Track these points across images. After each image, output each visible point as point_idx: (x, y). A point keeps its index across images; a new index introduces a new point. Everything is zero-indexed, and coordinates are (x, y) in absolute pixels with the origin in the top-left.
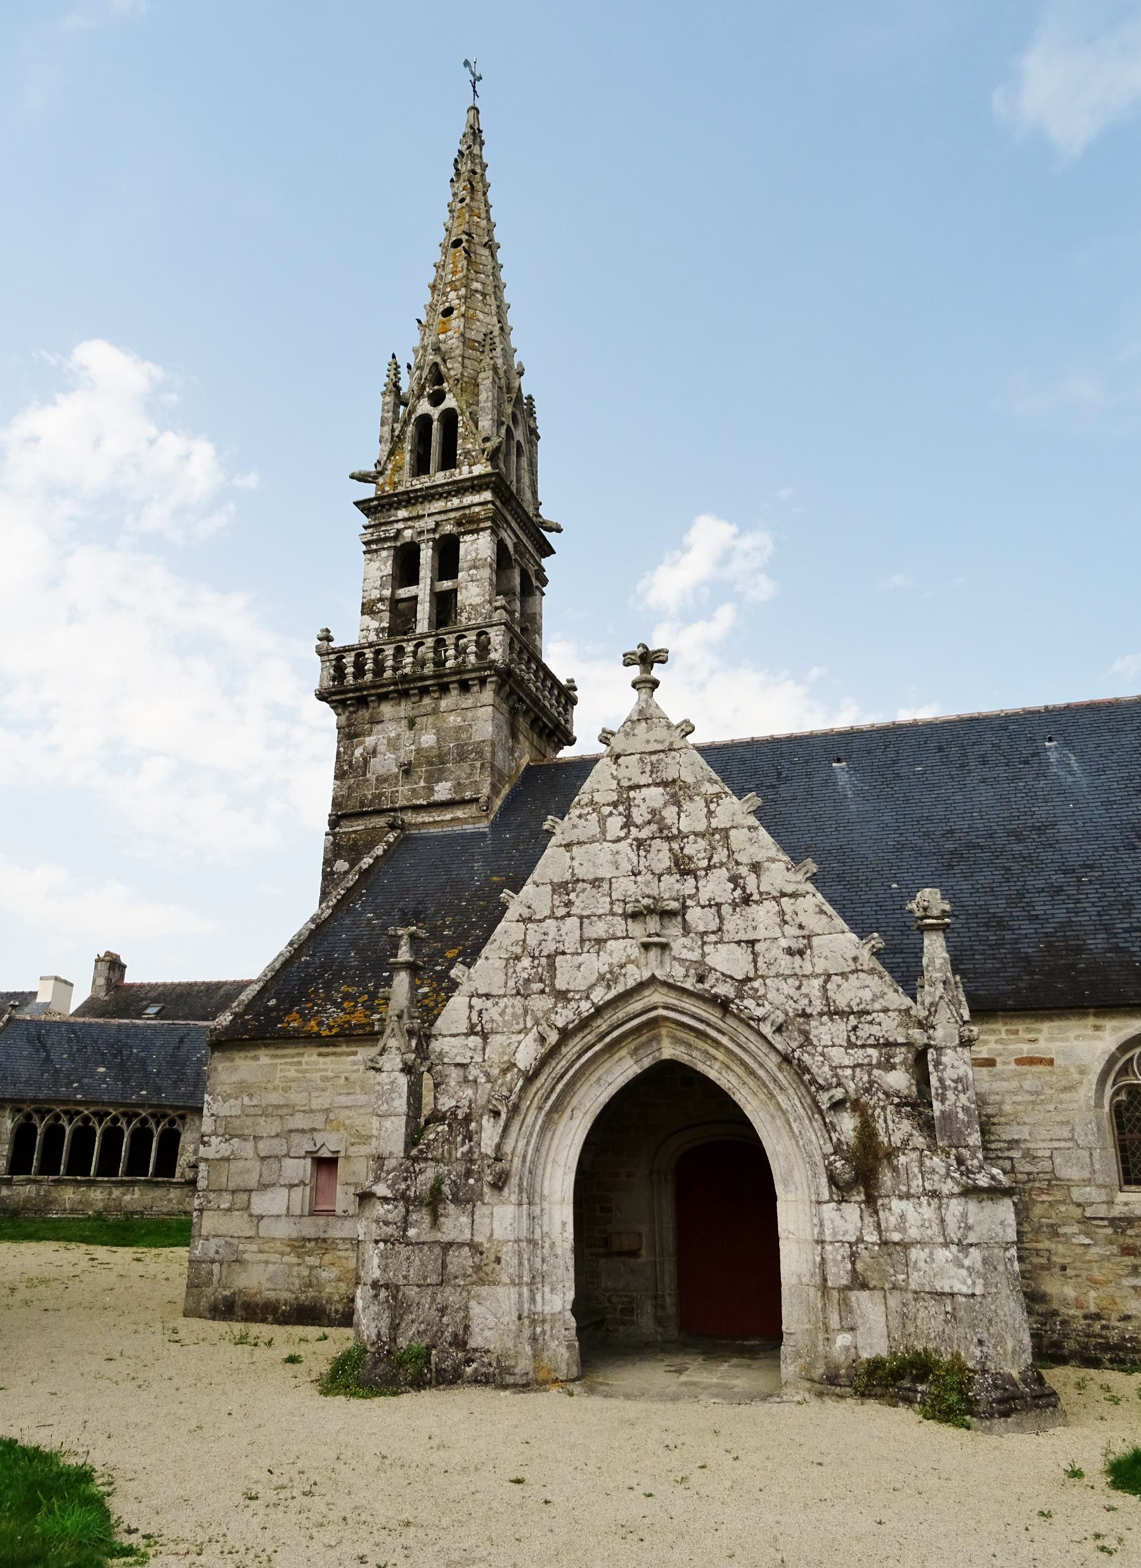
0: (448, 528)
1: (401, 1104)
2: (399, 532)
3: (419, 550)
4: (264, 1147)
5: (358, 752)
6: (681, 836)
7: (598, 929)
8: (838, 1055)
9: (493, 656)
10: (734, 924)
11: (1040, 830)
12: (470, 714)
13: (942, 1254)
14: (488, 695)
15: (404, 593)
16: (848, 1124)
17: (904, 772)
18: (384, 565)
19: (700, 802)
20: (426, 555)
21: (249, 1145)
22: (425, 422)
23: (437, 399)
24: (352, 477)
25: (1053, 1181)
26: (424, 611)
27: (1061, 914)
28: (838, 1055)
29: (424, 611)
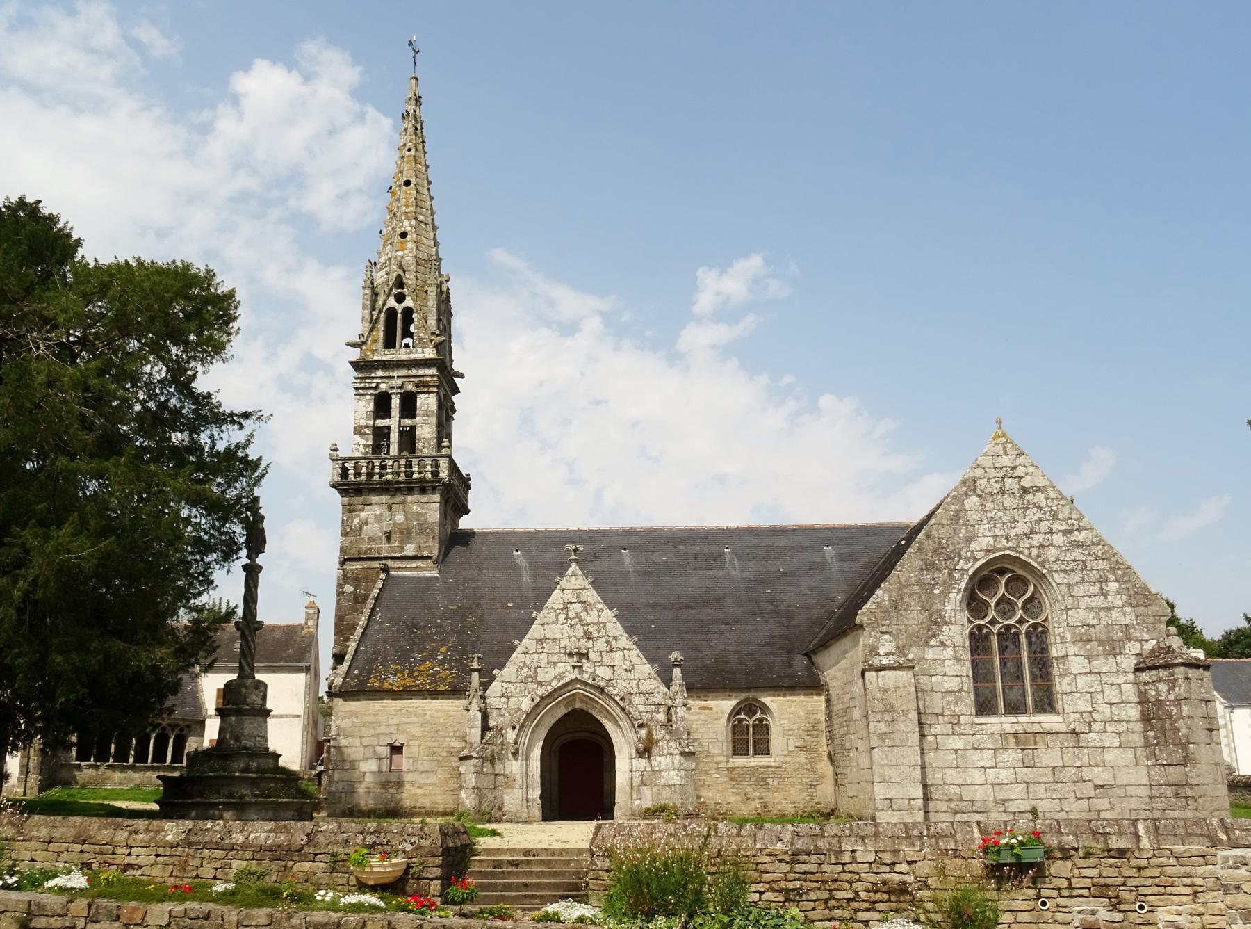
0: (410, 387)
1: (479, 723)
3: (390, 399)
4: (365, 741)
5: (356, 521)
6: (588, 624)
7: (555, 658)
8: (641, 708)
9: (441, 475)
10: (606, 659)
11: (718, 600)
12: (426, 506)
13: (672, 773)
14: (437, 497)
15: (381, 423)
16: (643, 732)
17: (658, 560)
18: (368, 405)
19: (595, 611)
20: (395, 402)
21: (357, 741)
22: (392, 313)
23: (400, 298)
24: (348, 344)
25: (709, 754)
26: (394, 437)
27: (722, 647)
28: (641, 708)
29: (394, 437)
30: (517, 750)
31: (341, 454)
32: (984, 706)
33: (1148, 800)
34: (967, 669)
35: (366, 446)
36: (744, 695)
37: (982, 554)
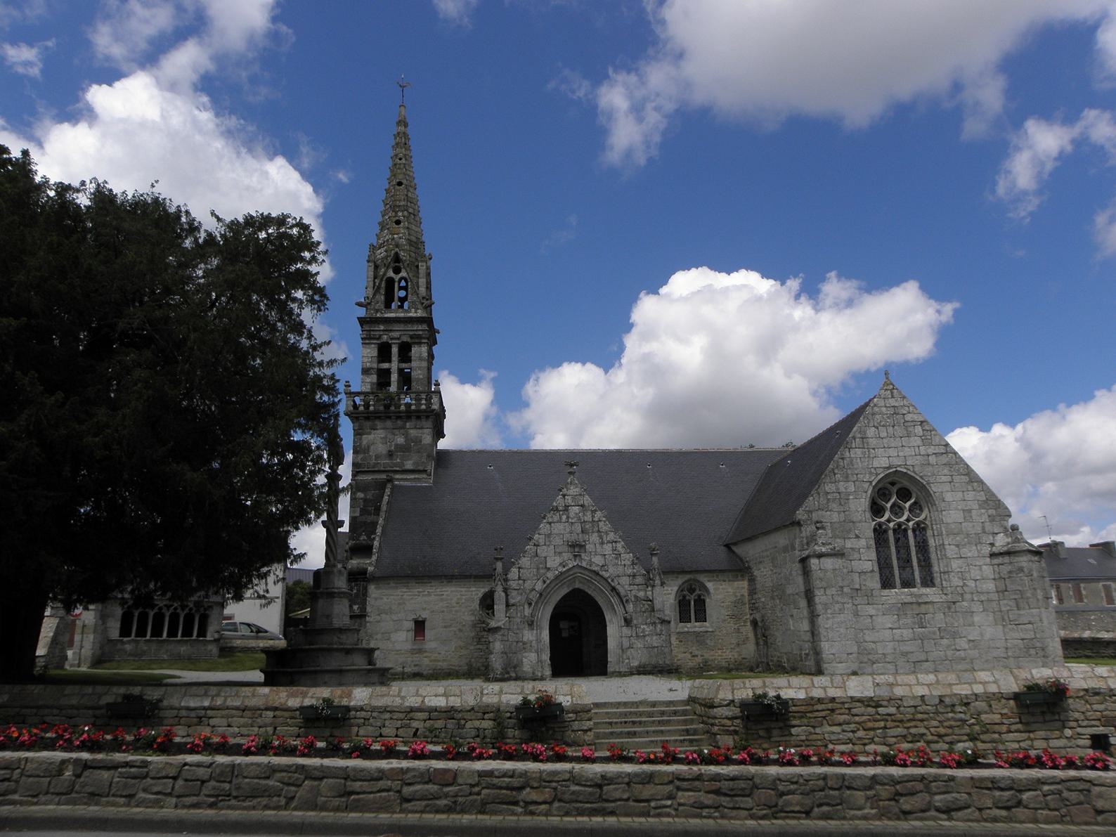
0: (405, 339)
2: (380, 336)
15: (386, 365)
18: (372, 351)
19: (590, 512)
20: (395, 350)
23: (397, 271)
26: (394, 377)
29: (394, 377)
30: (533, 622)
31: (353, 389)
32: (887, 583)
33: (1004, 650)
34: (873, 555)
35: (372, 384)
36: (688, 577)
37: (882, 470)
